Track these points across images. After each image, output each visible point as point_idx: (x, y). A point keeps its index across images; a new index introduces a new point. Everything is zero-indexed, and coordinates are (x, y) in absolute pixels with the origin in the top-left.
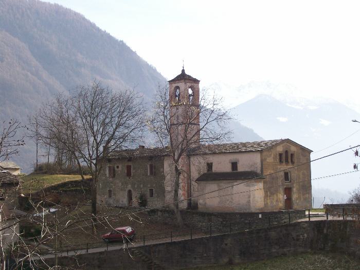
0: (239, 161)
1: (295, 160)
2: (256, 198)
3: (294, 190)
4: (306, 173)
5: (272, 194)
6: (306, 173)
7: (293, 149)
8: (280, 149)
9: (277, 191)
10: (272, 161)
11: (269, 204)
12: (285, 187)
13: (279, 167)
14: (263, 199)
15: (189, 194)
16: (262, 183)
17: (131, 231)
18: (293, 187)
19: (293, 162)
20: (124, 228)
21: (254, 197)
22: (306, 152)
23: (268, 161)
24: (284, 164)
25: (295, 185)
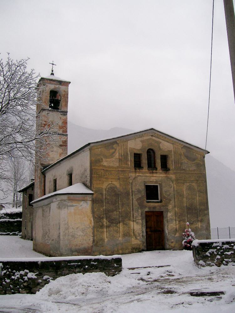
0: (145, 182)
1: (171, 164)
2: (71, 230)
3: (170, 215)
4: (196, 187)
5: (113, 222)
6: (196, 187)
7: (166, 147)
8: (136, 146)
9: (126, 217)
10: (117, 164)
11: (106, 240)
12: (147, 209)
13: (133, 175)
14: (90, 231)
15: (133, 227)
16: (90, 203)
17: (26, 285)
18: (167, 211)
19: (165, 167)
20: (230, 247)
21: (67, 229)
22: (195, 156)
23: (105, 164)
24: (145, 169)
25: (170, 207)
